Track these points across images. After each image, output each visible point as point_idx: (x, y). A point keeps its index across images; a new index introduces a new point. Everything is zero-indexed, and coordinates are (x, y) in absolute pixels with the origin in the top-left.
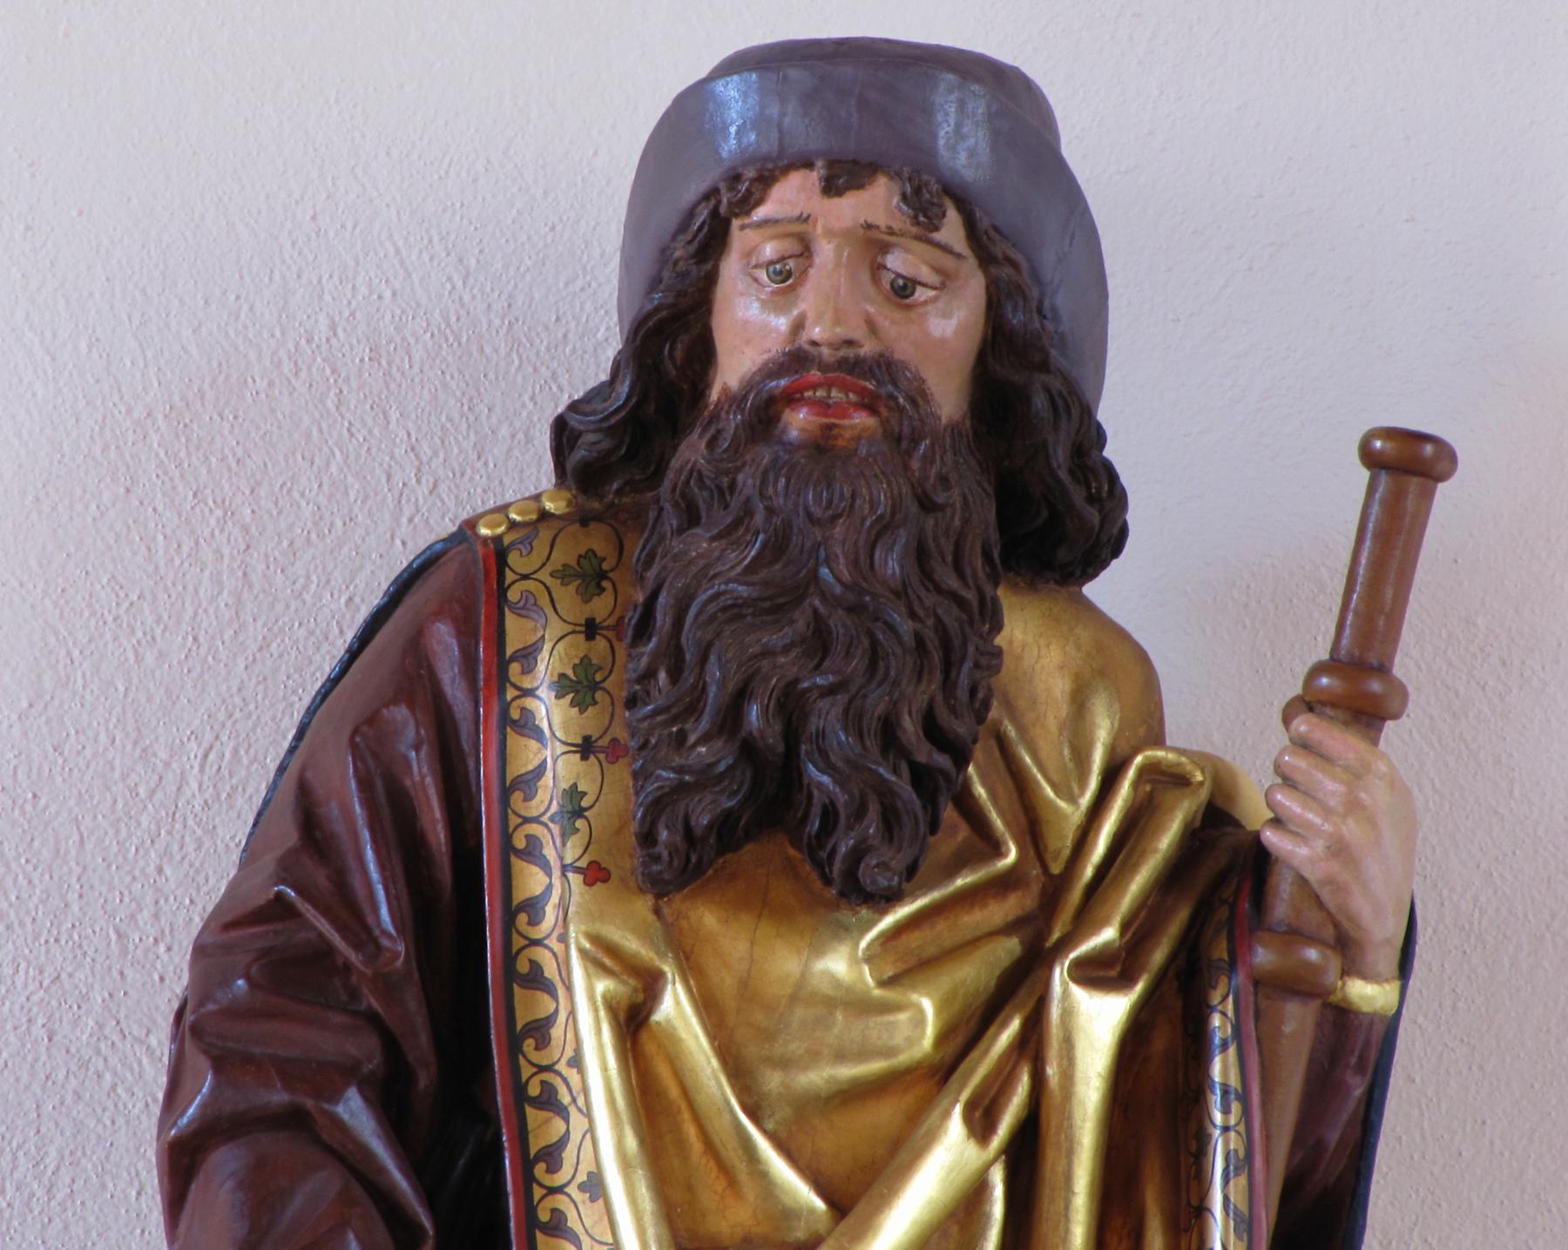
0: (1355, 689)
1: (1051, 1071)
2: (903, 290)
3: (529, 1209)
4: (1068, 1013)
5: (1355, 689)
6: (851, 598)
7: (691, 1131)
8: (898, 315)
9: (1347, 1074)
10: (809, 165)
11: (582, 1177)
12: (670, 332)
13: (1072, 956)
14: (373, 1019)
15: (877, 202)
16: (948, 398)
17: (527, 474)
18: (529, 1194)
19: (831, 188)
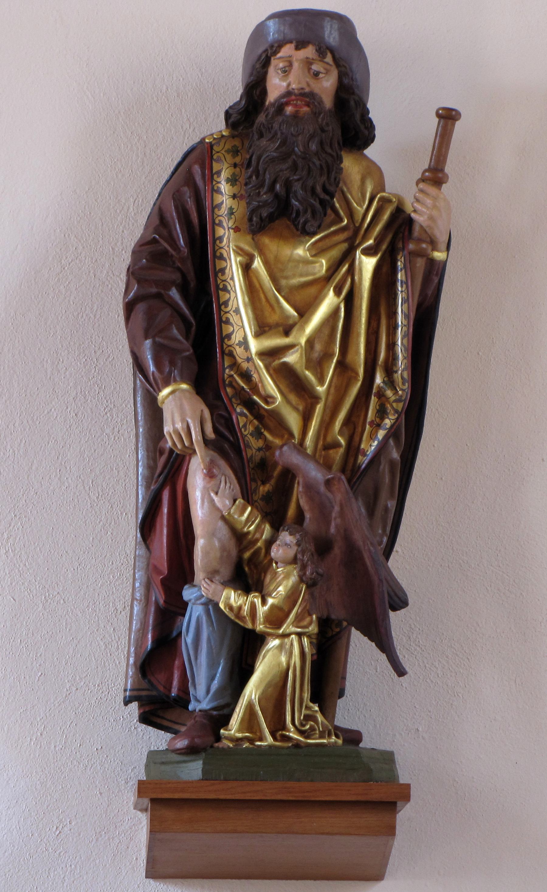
0: (435, 176)
1: (356, 278)
4: (361, 262)
5: (435, 176)
7: (262, 296)
10: (291, 42)
11: (234, 309)
12: (255, 87)
15: (309, 52)
16: (328, 102)
17: (219, 126)
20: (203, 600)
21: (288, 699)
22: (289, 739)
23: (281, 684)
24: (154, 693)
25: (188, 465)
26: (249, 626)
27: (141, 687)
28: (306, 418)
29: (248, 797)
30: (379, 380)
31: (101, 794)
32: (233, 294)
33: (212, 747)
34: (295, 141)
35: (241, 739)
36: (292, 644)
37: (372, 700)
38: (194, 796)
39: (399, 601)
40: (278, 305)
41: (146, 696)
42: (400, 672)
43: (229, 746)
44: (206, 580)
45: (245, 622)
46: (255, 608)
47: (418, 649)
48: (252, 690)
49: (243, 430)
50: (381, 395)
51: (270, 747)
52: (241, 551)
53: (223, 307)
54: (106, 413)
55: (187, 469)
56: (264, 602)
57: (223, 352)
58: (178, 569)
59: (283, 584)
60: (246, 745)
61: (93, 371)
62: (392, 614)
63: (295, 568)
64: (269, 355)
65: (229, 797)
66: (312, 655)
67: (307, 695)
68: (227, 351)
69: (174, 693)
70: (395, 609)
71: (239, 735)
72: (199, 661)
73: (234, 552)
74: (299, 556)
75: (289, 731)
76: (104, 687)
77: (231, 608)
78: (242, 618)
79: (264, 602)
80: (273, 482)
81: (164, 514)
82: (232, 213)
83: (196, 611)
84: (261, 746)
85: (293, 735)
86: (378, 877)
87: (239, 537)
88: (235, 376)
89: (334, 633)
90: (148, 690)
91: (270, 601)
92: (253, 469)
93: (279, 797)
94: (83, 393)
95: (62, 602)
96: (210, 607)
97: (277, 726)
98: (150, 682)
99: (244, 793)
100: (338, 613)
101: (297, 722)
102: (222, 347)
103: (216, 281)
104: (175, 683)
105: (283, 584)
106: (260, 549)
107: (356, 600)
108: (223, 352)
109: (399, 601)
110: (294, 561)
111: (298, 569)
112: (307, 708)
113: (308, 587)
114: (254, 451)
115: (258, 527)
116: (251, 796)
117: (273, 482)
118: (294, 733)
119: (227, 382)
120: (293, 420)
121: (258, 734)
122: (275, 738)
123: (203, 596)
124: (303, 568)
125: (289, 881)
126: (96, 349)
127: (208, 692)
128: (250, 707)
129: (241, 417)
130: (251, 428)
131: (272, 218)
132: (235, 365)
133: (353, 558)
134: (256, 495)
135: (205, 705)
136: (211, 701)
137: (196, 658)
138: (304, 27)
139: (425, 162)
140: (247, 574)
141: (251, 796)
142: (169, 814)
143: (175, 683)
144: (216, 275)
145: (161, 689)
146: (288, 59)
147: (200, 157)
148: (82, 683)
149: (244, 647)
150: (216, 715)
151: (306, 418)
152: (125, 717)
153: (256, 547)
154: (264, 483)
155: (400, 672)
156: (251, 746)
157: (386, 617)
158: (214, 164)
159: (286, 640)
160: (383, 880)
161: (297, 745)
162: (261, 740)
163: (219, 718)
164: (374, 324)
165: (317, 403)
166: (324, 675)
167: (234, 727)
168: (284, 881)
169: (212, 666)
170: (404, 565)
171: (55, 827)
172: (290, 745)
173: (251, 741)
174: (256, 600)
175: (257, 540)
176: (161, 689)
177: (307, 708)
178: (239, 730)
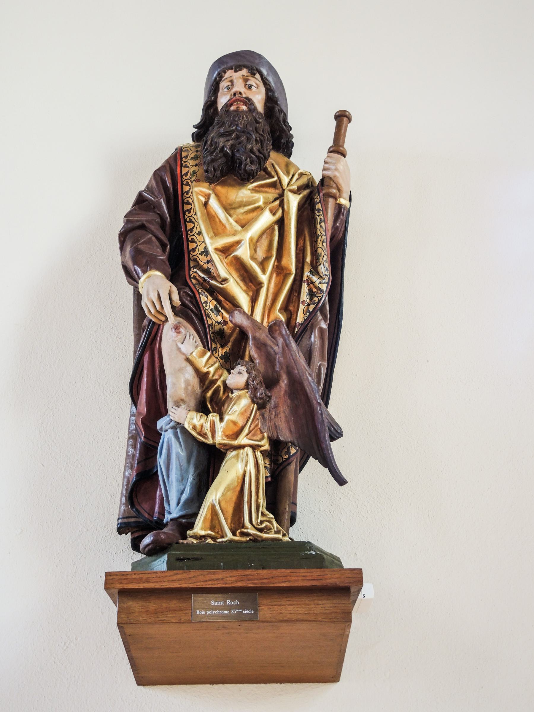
0: (337, 149)
1: (285, 207)
2: (250, 87)
3: (183, 200)
4: (287, 196)
5: (337, 149)
6: (243, 130)
7: (217, 220)
8: (250, 91)
9: (341, 214)
10: (232, 69)
11: (197, 232)
12: (210, 105)
13: (292, 277)
14: (158, 214)
15: (244, 72)
16: (260, 107)
17: (188, 141)
18: (187, 236)
19: (236, 71)
20: (172, 424)
21: (246, 499)
22: (248, 535)
23: (239, 488)
24: (141, 520)
25: (162, 331)
26: (210, 441)
27: (130, 515)
28: (254, 300)
29: (209, 585)
30: (307, 274)
31: (102, 613)
32: (196, 224)
33: (177, 543)
34: (242, 134)
35: (205, 537)
36: (247, 455)
37: (324, 514)
38: (158, 586)
39: (336, 434)
40: (234, 227)
41: (134, 522)
42: (341, 481)
43: (193, 542)
44: (174, 407)
45: (206, 438)
46: (217, 429)
47: (350, 493)
48: (216, 494)
49: (204, 305)
50: (310, 282)
51: (231, 541)
52: (205, 391)
53: (189, 232)
54: (118, 340)
55: (161, 334)
56: (221, 419)
57: (189, 259)
58: (157, 406)
59: (240, 407)
60: (209, 541)
61: (109, 315)
62: (332, 443)
63: (247, 392)
64: (225, 251)
65: (191, 585)
66: (266, 477)
67: (262, 501)
68: (192, 258)
69: (156, 515)
70: (332, 439)
71: (203, 533)
72: (170, 479)
73: (198, 390)
74: (250, 382)
75: (247, 528)
76: (109, 529)
77: (194, 428)
78: (204, 435)
79: (221, 419)
80: (230, 345)
81: (148, 383)
82: (195, 173)
83: (168, 436)
84: (222, 542)
85: (252, 531)
86: (335, 678)
87: (203, 377)
88: (198, 271)
89: (284, 459)
90: (136, 517)
91: (227, 418)
92: (212, 333)
93: (239, 584)
94: (102, 328)
95: (79, 466)
96: (178, 430)
97: (237, 524)
98: (137, 510)
99: (206, 581)
100: (285, 435)
101: (254, 522)
102: (189, 256)
103: (184, 217)
104: (157, 509)
105: (240, 407)
106: (219, 387)
107: (304, 435)
108: (189, 259)
109: (336, 434)
110: (247, 386)
111: (249, 393)
112: (263, 514)
113: (259, 408)
114: (214, 322)
115: (216, 370)
116: (212, 584)
117: (230, 345)
118: (251, 529)
119: (192, 276)
120: (243, 299)
121: (220, 533)
122: (234, 534)
123: (172, 420)
124: (255, 390)
125: (259, 685)
126: (112, 302)
127: (178, 504)
128: (213, 507)
129: (208, 302)
130: (212, 307)
131: (223, 174)
132: (198, 266)
133: (297, 389)
134: (216, 353)
135: (175, 515)
136: (180, 510)
137: (168, 477)
138: (245, 61)
139: (330, 143)
140: (211, 401)
141: (212, 584)
142: (135, 605)
143: (157, 509)
144: (184, 213)
145: (146, 515)
146: (230, 79)
147: (178, 156)
148: (92, 526)
149: (209, 459)
150: (185, 522)
151: (254, 300)
152: (124, 550)
153: (216, 386)
154: (222, 346)
155: (341, 481)
156: (213, 542)
157: (330, 444)
158: (183, 153)
159: (242, 451)
160: (339, 681)
161: (255, 540)
162: (222, 537)
163: (185, 523)
164: (301, 243)
165: (262, 287)
166: (278, 495)
167: (200, 528)
168: (255, 685)
169: (182, 479)
170: (338, 409)
171: (63, 643)
172: (248, 539)
173: (214, 538)
174: (214, 418)
175: (217, 380)
176: (146, 515)
177: (263, 514)
178: (202, 529)
